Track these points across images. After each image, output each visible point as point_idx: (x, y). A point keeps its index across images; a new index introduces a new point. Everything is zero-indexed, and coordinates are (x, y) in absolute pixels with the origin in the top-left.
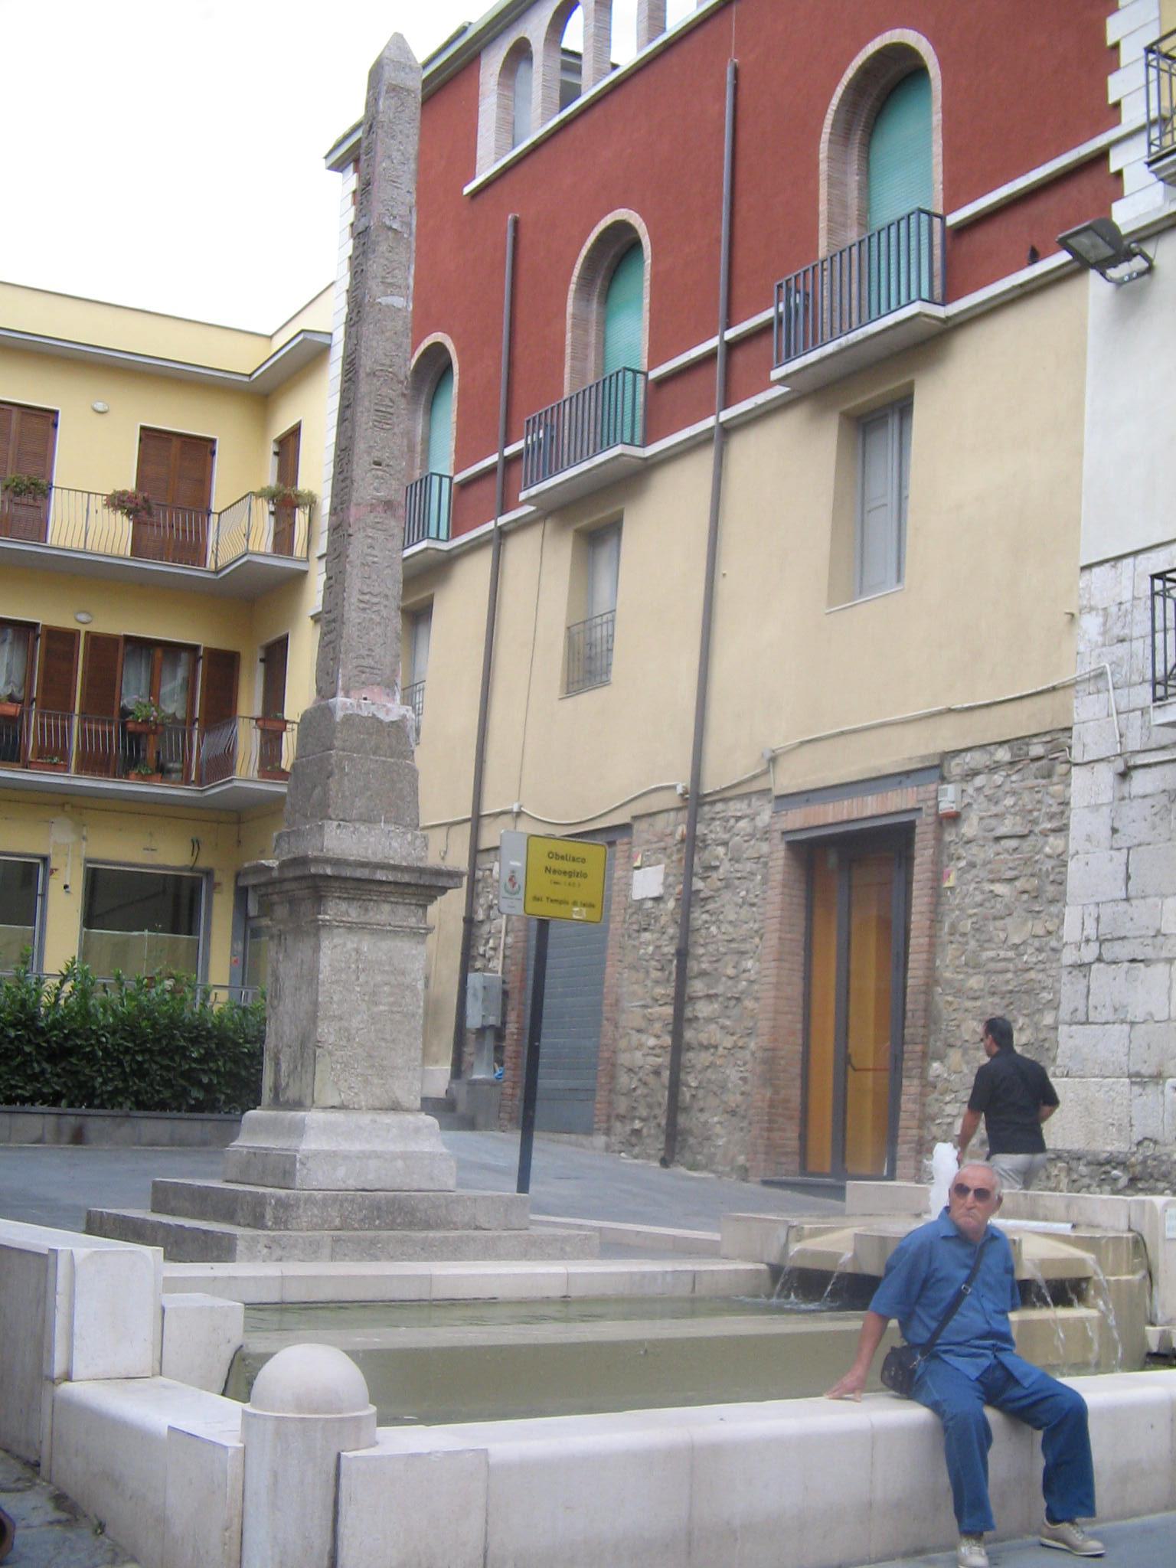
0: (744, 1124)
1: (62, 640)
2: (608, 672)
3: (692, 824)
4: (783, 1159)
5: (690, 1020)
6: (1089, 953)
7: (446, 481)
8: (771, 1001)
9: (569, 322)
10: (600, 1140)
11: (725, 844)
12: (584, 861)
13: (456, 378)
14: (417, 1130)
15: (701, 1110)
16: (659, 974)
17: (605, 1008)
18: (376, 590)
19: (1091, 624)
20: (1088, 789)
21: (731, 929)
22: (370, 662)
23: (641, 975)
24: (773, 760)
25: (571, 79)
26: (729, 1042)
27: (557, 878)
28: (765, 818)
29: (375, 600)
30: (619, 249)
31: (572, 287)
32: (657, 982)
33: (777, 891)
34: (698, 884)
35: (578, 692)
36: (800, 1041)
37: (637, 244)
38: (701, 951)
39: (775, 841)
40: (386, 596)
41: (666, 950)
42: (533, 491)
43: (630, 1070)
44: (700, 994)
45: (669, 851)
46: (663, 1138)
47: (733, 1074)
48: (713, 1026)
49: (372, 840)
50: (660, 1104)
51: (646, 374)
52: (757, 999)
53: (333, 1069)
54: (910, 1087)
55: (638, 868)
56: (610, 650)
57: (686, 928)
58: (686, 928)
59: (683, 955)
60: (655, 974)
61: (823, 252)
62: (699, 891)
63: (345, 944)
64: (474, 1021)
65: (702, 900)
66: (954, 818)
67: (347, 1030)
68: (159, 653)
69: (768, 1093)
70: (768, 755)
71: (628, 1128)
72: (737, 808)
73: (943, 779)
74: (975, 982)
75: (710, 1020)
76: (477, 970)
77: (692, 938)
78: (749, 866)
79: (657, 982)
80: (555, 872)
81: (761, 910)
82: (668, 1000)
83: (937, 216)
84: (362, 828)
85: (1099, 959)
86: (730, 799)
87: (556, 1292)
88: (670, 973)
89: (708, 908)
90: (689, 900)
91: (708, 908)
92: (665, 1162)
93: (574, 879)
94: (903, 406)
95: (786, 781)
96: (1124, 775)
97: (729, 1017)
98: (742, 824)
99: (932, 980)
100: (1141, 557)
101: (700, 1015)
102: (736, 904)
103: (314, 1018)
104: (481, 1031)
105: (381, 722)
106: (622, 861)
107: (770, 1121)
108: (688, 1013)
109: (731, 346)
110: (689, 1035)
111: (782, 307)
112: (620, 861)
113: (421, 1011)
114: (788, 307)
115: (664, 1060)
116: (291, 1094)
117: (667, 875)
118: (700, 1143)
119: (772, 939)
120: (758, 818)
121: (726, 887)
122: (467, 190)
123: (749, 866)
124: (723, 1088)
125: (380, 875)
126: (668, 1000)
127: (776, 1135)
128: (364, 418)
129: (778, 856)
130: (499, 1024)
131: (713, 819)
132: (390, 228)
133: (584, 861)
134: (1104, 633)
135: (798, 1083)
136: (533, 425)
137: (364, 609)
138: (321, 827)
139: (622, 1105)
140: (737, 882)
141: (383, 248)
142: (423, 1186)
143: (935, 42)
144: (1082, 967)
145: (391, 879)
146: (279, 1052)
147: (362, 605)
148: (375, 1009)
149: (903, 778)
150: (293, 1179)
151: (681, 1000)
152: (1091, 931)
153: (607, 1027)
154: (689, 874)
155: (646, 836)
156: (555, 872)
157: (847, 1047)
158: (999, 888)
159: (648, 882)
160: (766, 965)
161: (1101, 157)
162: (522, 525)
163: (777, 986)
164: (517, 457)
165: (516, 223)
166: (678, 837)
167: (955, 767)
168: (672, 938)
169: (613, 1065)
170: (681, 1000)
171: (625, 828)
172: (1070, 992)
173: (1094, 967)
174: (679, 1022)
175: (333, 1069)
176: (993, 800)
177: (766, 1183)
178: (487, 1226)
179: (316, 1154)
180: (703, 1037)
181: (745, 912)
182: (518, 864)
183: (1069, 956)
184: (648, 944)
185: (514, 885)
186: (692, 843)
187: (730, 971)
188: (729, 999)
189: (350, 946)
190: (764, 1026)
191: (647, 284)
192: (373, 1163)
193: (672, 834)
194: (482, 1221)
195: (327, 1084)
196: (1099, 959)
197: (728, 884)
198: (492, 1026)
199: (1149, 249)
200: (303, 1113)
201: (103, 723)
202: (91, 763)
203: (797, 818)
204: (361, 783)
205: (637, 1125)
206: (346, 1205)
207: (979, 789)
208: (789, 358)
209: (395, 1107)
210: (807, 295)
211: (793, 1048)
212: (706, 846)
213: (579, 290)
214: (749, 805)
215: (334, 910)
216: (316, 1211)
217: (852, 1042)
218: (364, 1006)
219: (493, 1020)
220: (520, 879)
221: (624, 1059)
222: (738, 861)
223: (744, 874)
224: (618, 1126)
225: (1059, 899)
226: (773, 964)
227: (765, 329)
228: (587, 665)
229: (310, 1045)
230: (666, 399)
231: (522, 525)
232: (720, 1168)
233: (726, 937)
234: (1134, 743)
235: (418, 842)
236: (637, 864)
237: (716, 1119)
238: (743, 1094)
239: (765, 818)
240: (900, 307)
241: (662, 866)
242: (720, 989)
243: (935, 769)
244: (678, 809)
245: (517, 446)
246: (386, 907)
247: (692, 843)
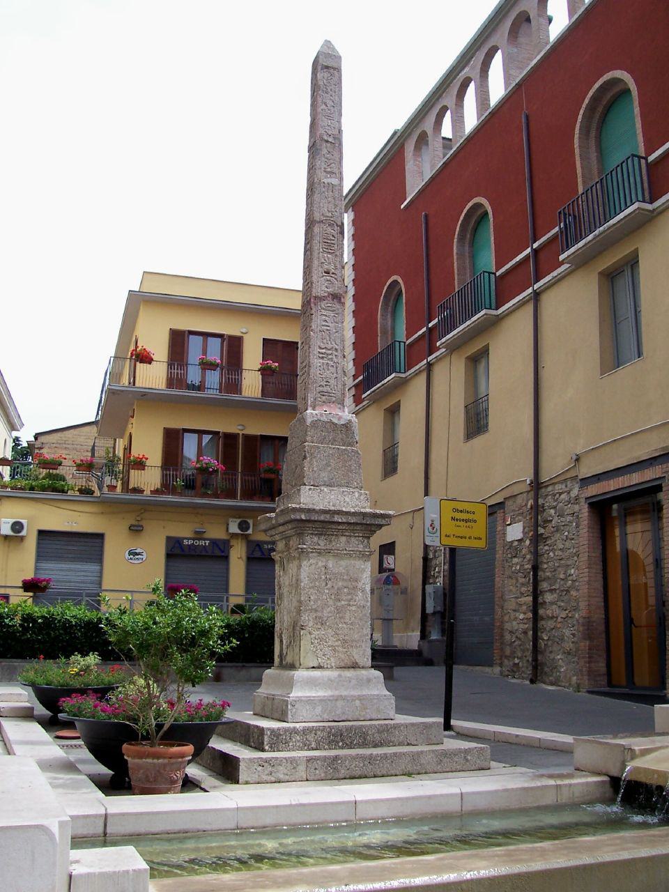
0: (576, 659)
1: (230, 439)
2: (487, 426)
3: (536, 500)
4: (598, 679)
5: (541, 603)
7: (402, 344)
8: (586, 591)
9: (455, 257)
11: (554, 508)
12: (474, 513)
13: (404, 295)
14: (369, 680)
15: (551, 652)
16: (524, 580)
17: (496, 599)
18: (329, 346)
21: (560, 553)
22: (328, 389)
23: (514, 581)
24: (577, 460)
26: (563, 614)
27: (458, 523)
29: (330, 352)
30: (477, 219)
31: (455, 240)
32: (523, 584)
33: (585, 530)
34: (541, 531)
35: (472, 438)
36: (603, 612)
37: (486, 213)
38: (545, 566)
39: (582, 504)
40: (336, 350)
41: (526, 567)
42: (443, 340)
43: (511, 632)
44: (546, 589)
45: (525, 514)
46: (530, 668)
47: (567, 632)
48: (554, 607)
49: (332, 497)
50: (528, 650)
51: (495, 274)
52: (578, 590)
53: (312, 643)
55: (509, 525)
56: (487, 415)
57: (536, 554)
58: (536, 554)
59: (535, 568)
60: (522, 580)
61: (581, 190)
62: (542, 534)
63: (317, 563)
64: (429, 610)
65: (544, 538)
67: (320, 618)
68: (277, 442)
69: (588, 643)
70: (574, 457)
71: (511, 663)
72: (558, 488)
75: (552, 603)
76: (431, 584)
77: (540, 560)
78: (569, 518)
79: (523, 584)
80: (457, 520)
81: (577, 542)
82: (529, 593)
83: (643, 158)
84: (325, 489)
86: (556, 483)
87: (455, 806)
88: (529, 579)
89: (548, 543)
90: (537, 539)
91: (548, 543)
92: (532, 681)
93: (468, 524)
95: (586, 471)
97: (562, 601)
98: (563, 496)
101: (547, 601)
102: (563, 540)
103: (299, 612)
104: (434, 613)
105: (336, 424)
106: (500, 522)
107: (589, 657)
108: (540, 600)
109: (535, 251)
110: (541, 612)
111: (562, 225)
112: (500, 522)
113: (369, 604)
114: (565, 224)
115: (529, 625)
116: (289, 659)
117: (524, 528)
118: (551, 670)
119: (584, 557)
120: (571, 492)
121: (557, 531)
122: (402, 207)
123: (569, 518)
124: (562, 639)
125: (337, 518)
126: (529, 593)
127: (593, 665)
128: (317, 246)
130: (443, 611)
131: (547, 495)
132: (327, 141)
133: (474, 513)
135: (604, 635)
136: (443, 308)
137: (323, 358)
138: (299, 490)
139: (508, 651)
140: (562, 528)
141: (325, 151)
142: (374, 717)
143: (630, 72)
145: (344, 520)
146: (282, 633)
147: (321, 355)
149: (652, 461)
150: (287, 716)
151: (536, 594)
153: (498, 610)
154: (536, 525)
155: (512, 508)
156: (457, 520)
157: (630, 614)
159: (515, 532)
160: (581, 571)
162: (439, 359)
163: (589, 583)
165: (426, 216)
166: (529, 506)
168: (529, 560)
169: (502, 629)
170: (536, 594)
175: (312, 643)
177: (589, 692)
178: (415, 743)
179: (299, 700)
180: (549, 613)
181: (568, 544)
182: (435, 516)
184: (517, 564)
185: (433, 529)
186: (537, 509)
187: (562, 576)
188: (562, 591)
189: (320, 564)
190: (583, 605)
191: (492, 230)
192: (340, 703)
193: (526, 505)
194: (412, 739)
198: (439, 612)
200: (294, 672)
201: (251, 476)
202: (248, 495)
204: (324, 463)
205: (516, 661)
206: (319, 733)
208: (568, 248)
209: (355, 666)
210: (575, 217)
211: (599, 616)
212: (544, 510)
213: (458, 242)
214: (566, 486)
216: (298, 738)
217: (633, 612)
218: (331, 602)
219: (439, 609)
220: (437, 524)
221: (507, 626)
222: (562, 516)
223: (566, 523)
224: (506, 662)
226: (587, 570)
228: (476, 422)
229: (298, 628)
231: (439, 359)
232: (563, 684)
233: (558, 558)
235: (362, 497)
236: (508, 523)
237: (559, 657)
238: (573, 642)
239: (575, 492)
240: (627, 207)
241: (521, 524)
242: (557, 586)
244: (528, 492)
246: (343, 539)
247: (537, 509)
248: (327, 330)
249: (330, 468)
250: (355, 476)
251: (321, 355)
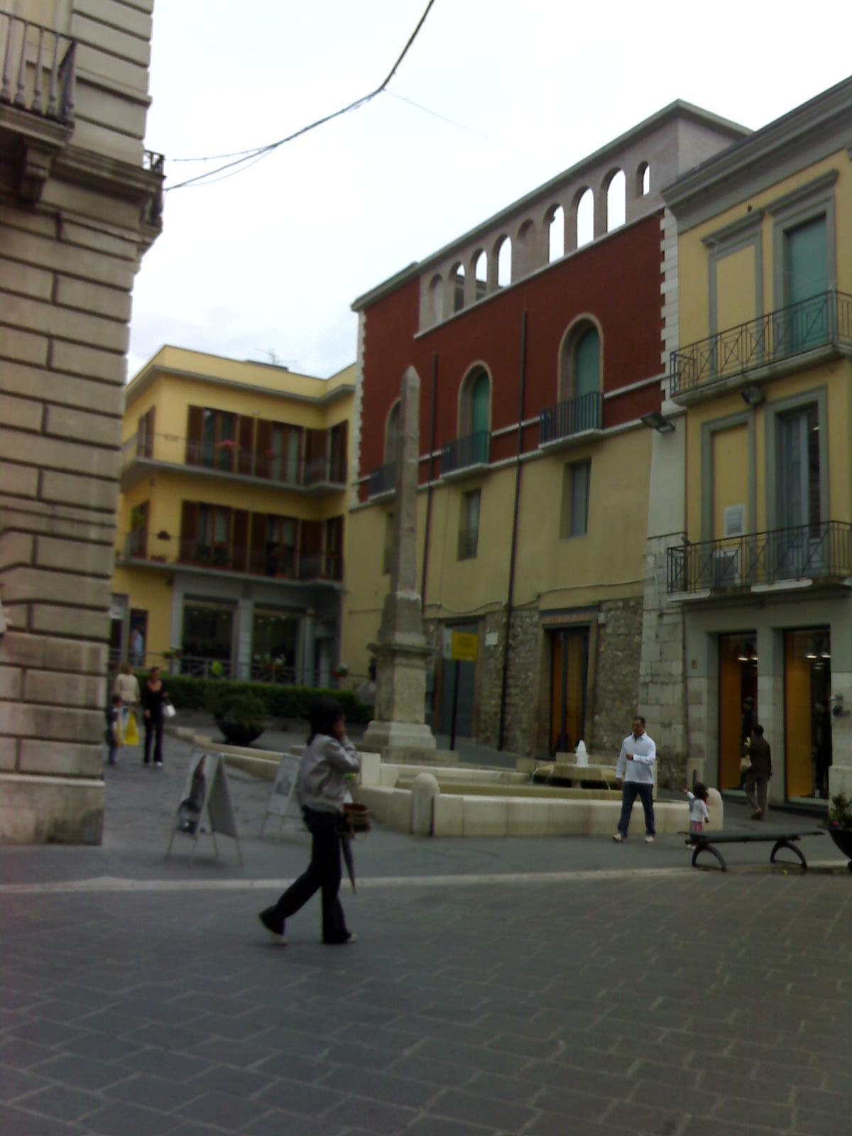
1: (241, 515)
6: (648, 679)
10: (473, 740)
19: (651, 560)
20: (649, 619)
25: (460, 286)
28: (536, 618)
37: (485, 375)
54: (588, 725)
59: (505, 669)
66: (604, 626)
72: (525, 613)
73: (600, 611)
74: (610, 687)
85: (652, 682)
90: (508, 647)
94: (587, 464)
95: (546, 604)
96: (661, 616)
98: (528, 620)
99: (595, 685)
100: (668, 537)
109: (524, 429)
114: (545, 417)
129: (541, 633)
134: (655, 563)
144: (646, 684)
151: (505, 686)
152: (649, 671)
154: (507, 638)
158: (619, 653)
159: (492, 639)
161: (658, 383)
164: (438, 457)
167: (604, 607)
170: (505, 686)
171: (483, 617)
172: (642, 693)
173: (650, 685)
174: (504, 695)
176: (617, 620)
183: (641, 680)
195: (398, 713)
196: (652, 682)
197: (523, 643)
199: (673, 422)
203: (547, 620)
205: (488, 734)
207: (612, 616)
215: (399, 660)
225: (639, 659)
227: (536, 424)
228: (467, 548)
230: (498, 447)
231: (439, 487)
234: (664, 605)
243: (597, 607)
245: (437, 453)
247: (508, 626)
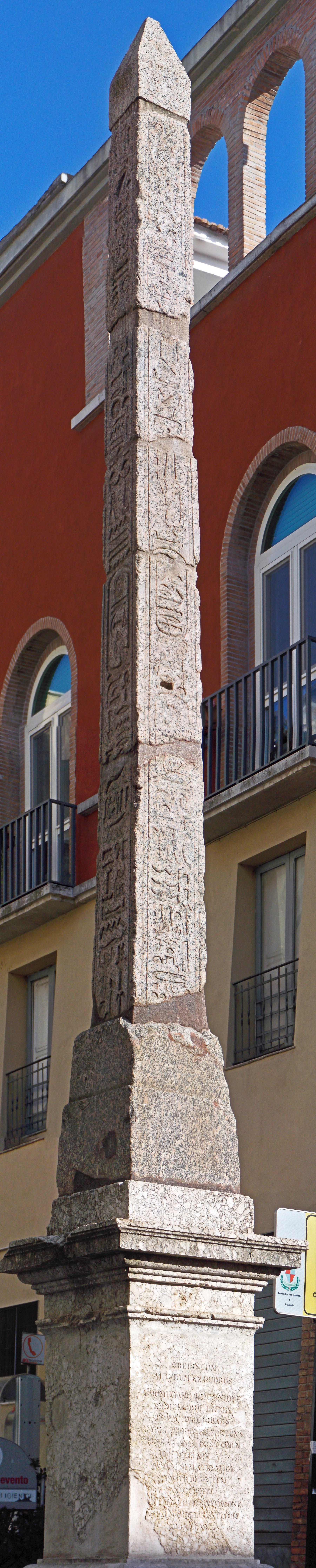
22: (169, 965)
49: (187, 1205)
137: (160, 893)
147: (157, 888)
148: (200, 1428)
248: (169, 828)
249: (178, 1142)
250: (226, 1162)
251: (157, 888)
